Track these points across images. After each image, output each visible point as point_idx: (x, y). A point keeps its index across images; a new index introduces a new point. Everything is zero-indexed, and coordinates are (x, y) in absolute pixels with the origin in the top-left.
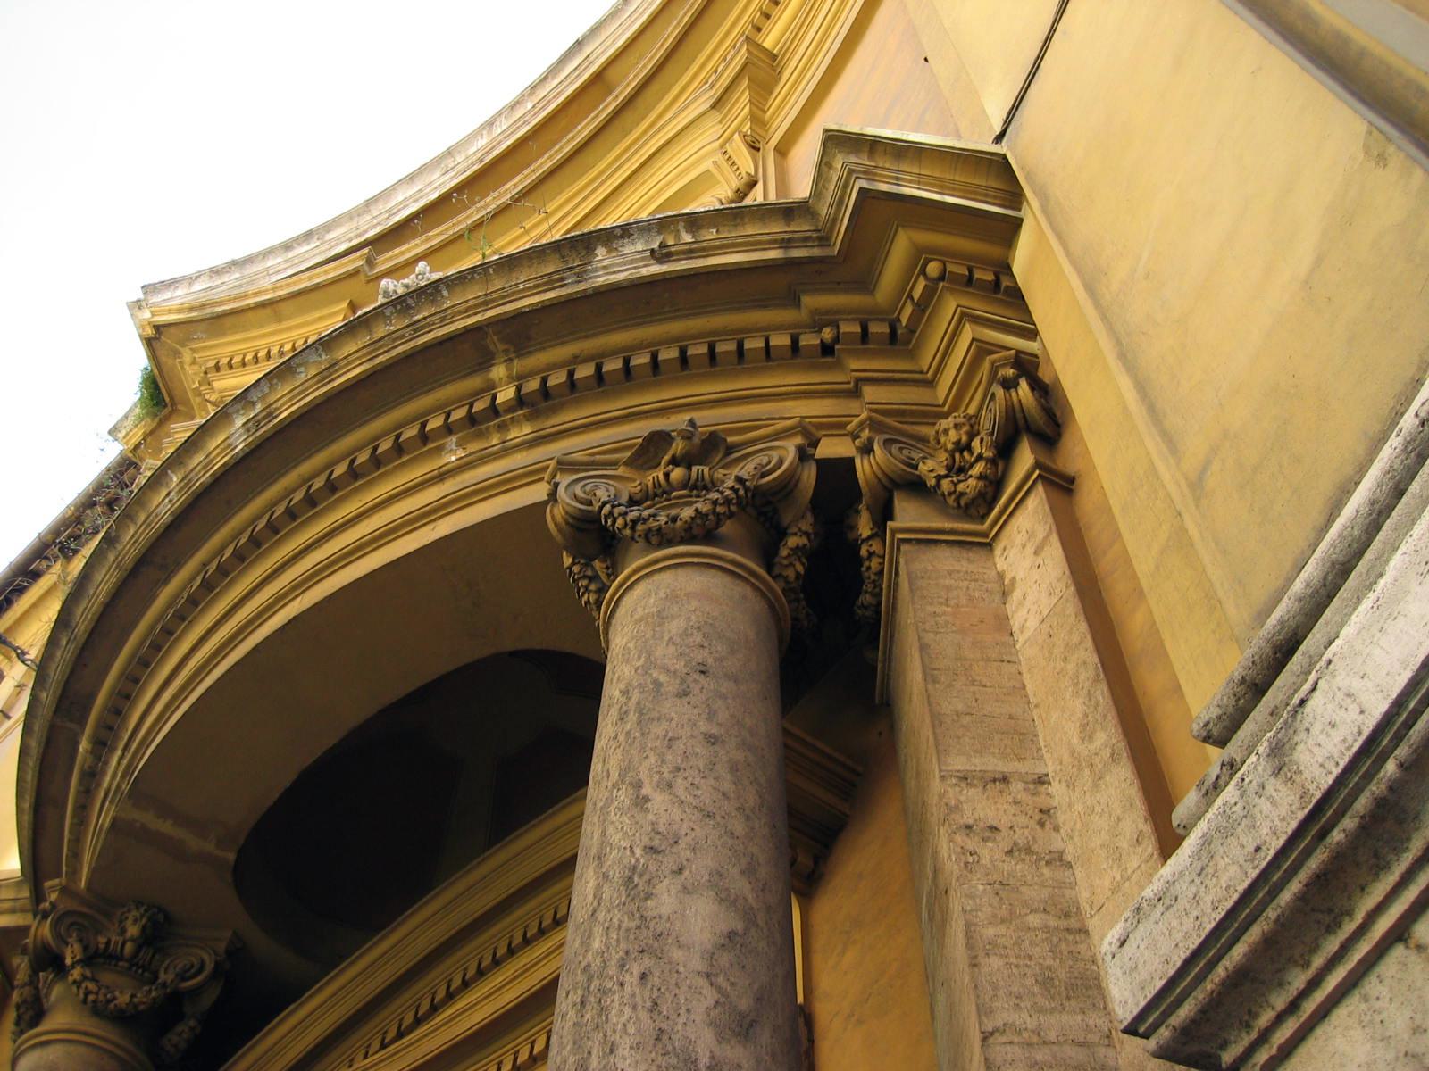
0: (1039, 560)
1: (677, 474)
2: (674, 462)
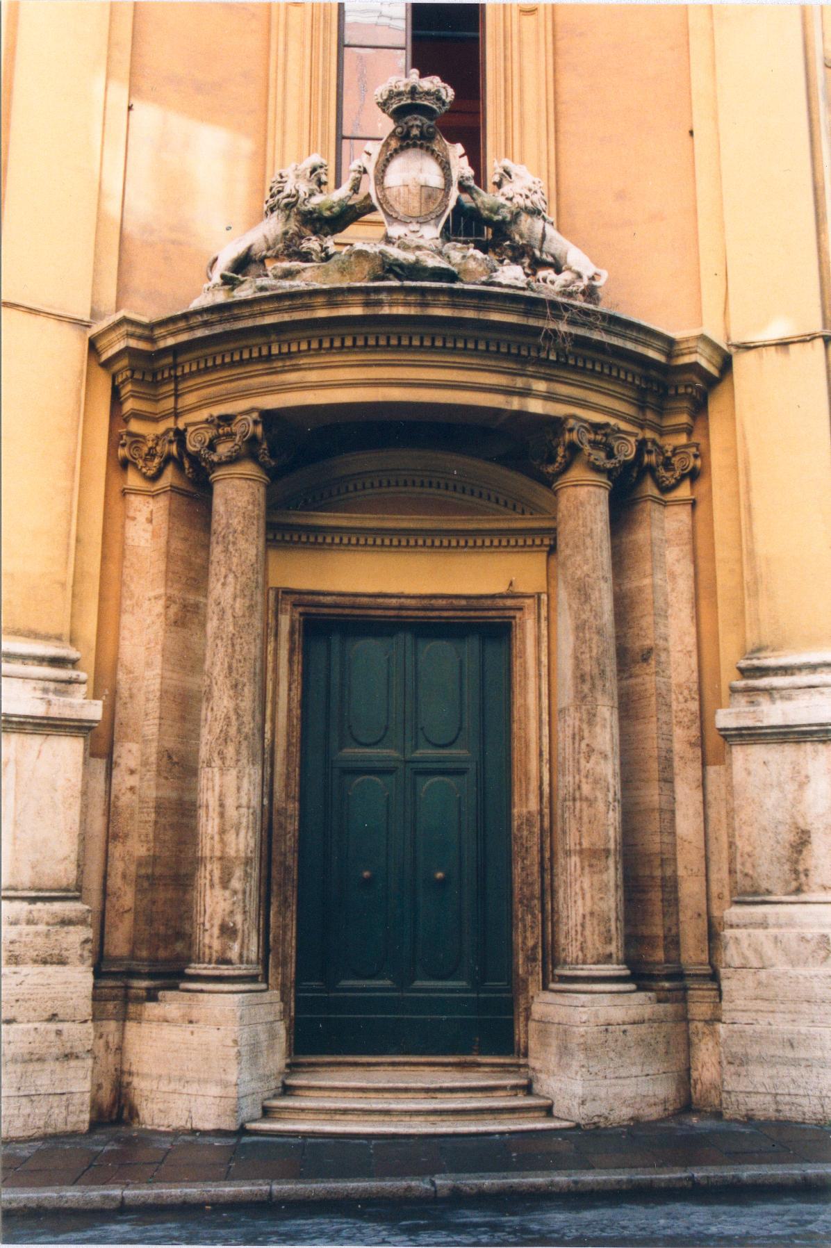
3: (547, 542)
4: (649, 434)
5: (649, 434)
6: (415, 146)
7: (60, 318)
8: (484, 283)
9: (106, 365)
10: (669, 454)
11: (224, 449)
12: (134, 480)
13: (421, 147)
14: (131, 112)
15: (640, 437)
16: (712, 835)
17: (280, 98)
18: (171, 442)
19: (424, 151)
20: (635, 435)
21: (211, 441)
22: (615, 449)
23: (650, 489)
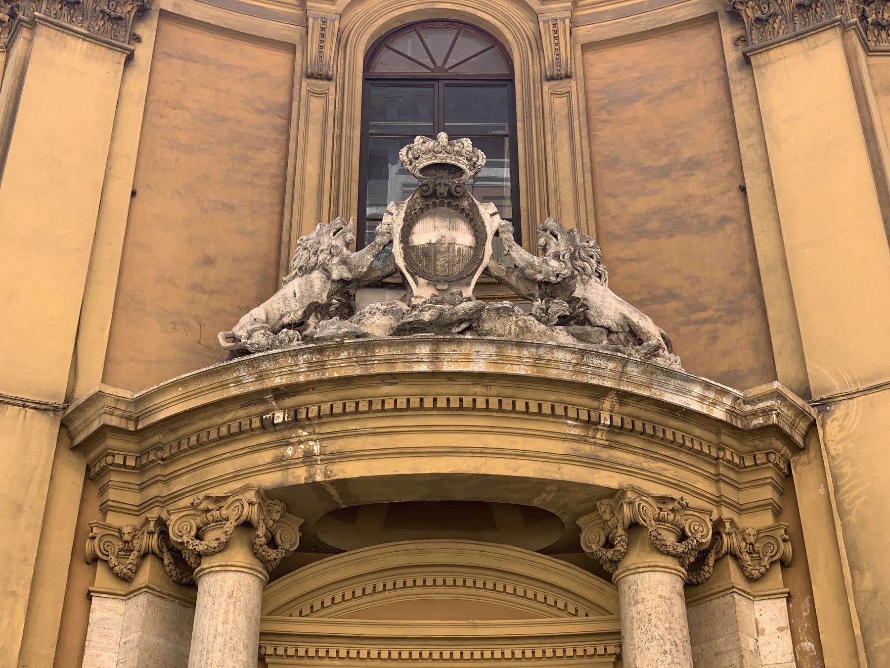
0: (780, 634)
1: (671, 517)
2: (673, 510)
3: (611, 650)
4: (726, 513)
5: (726, 513)
6: (442, 204)
7: (24, 404)
8: (727, 393)
9: (80, 449)
10: (752, 539)
11: (212, 538)
12: (102, 579)
13: (449, 205)
14: (135, 199)
15: (715, 517)
16: (287, 249)
17: (421, 596)
18: (151, 533)
19: (452, 211)
20: (710, 513)
21: (199, 529)
22: (687, 530)
23: (734, 575)
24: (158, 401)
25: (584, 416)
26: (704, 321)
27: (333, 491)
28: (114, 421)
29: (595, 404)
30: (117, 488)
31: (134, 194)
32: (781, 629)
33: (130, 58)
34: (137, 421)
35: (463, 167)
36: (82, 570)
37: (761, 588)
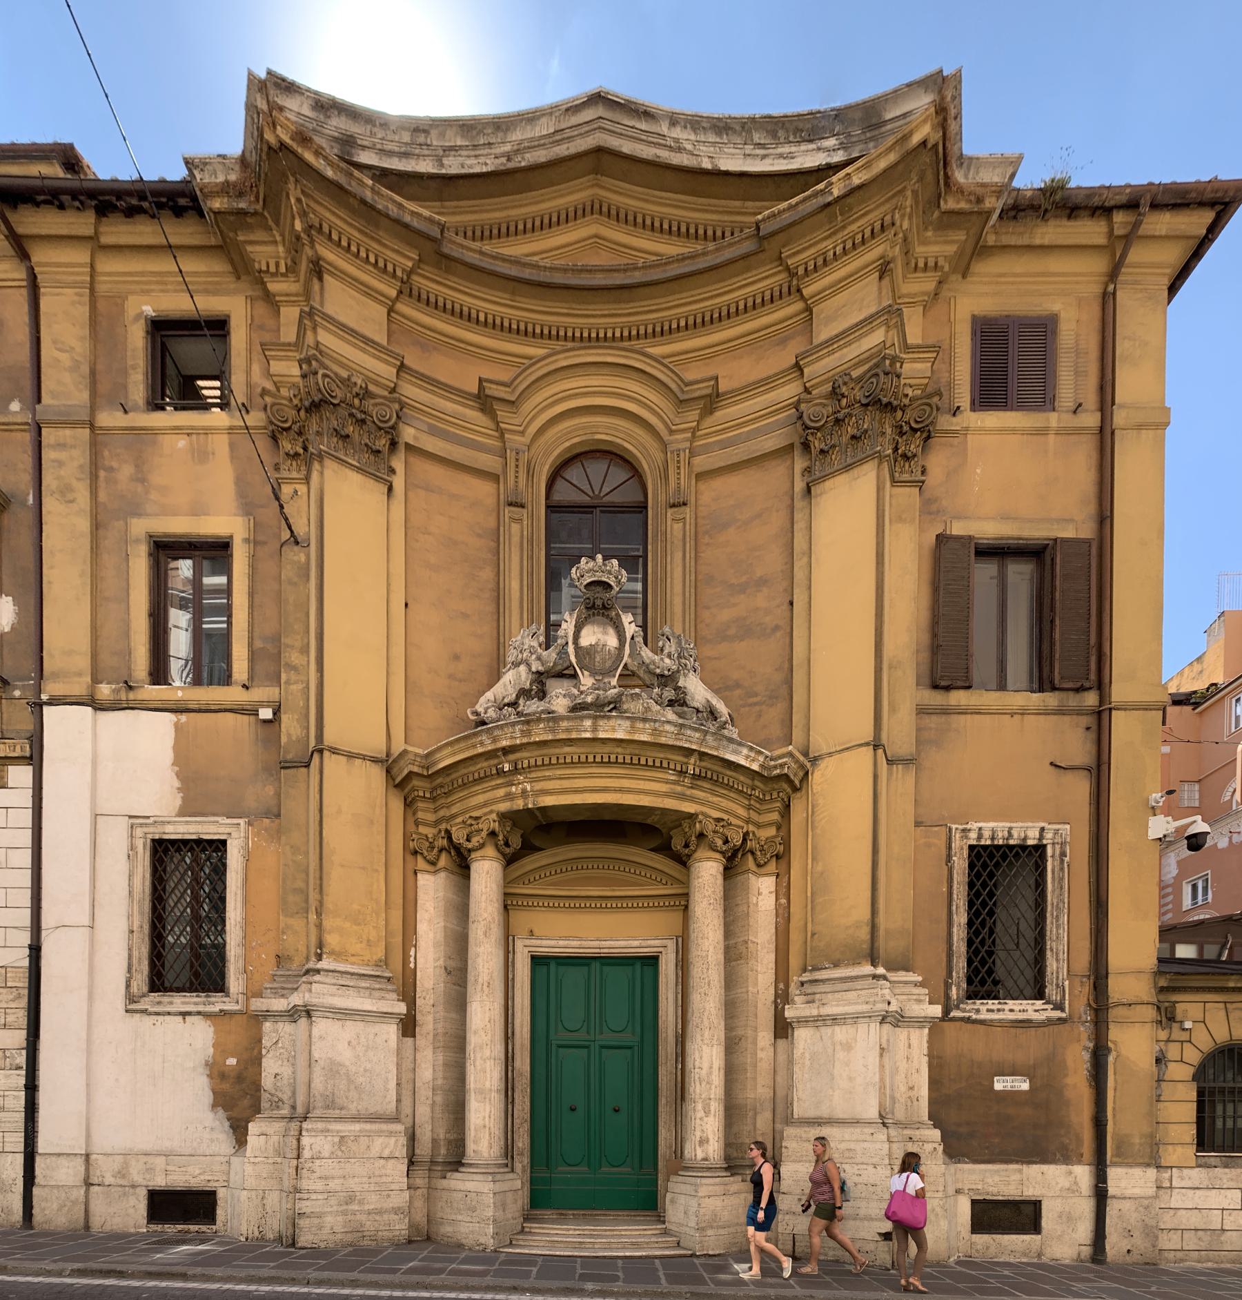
24: (438, 756)
25: (679, 768)
26: (755, 704)
27: (538, 814)
28: (416, 769)
29: (685, 760)
30: (422, 810)
31: (406, 605)
32: (771, 893)
33: (390, 489)
34: (428, 769)
35: (612, 583)
36: (410, 858)
37: (763, 870)
